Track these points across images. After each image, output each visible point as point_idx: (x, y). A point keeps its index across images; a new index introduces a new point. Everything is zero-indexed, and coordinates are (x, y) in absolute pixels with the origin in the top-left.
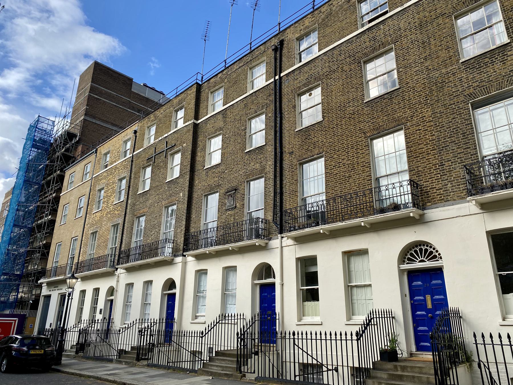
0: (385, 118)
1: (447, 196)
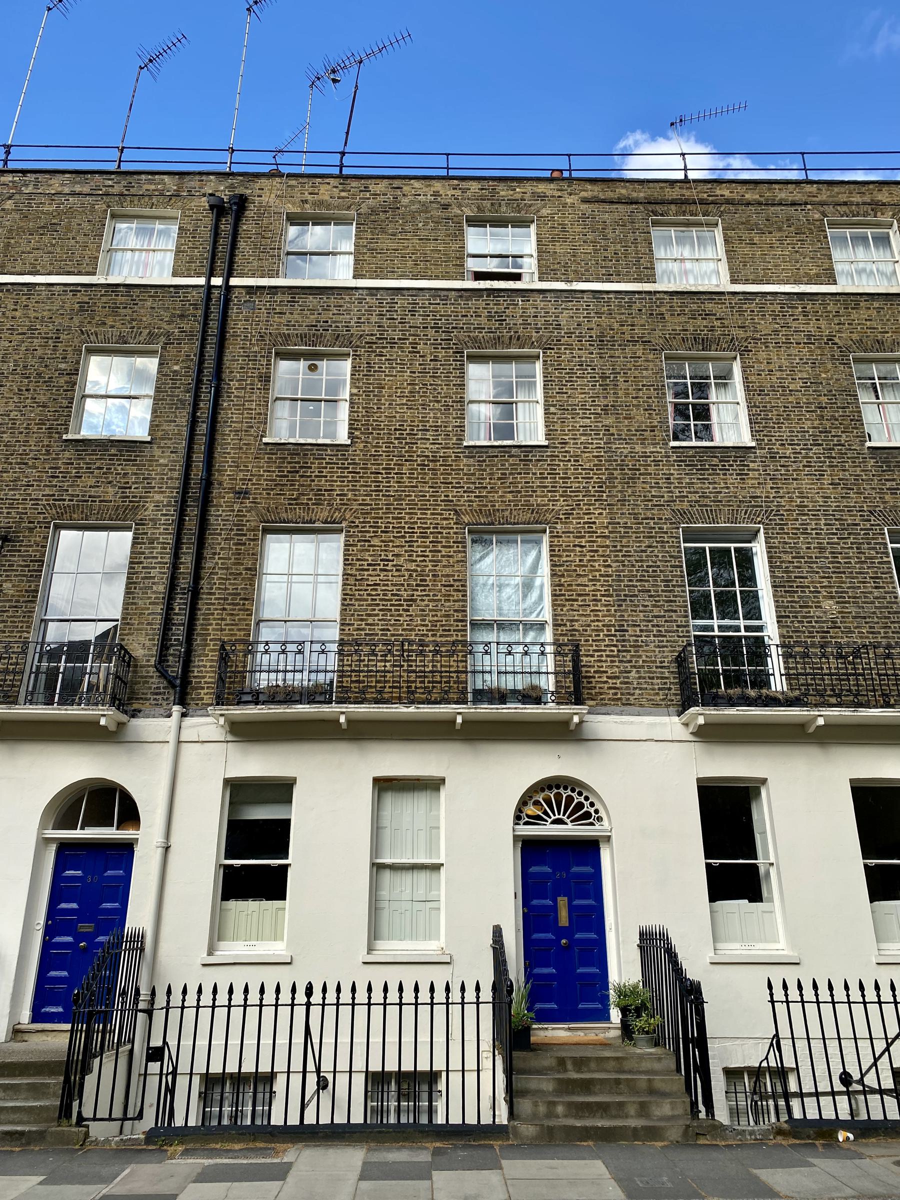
0: (510, 496)
1: (629, 694)
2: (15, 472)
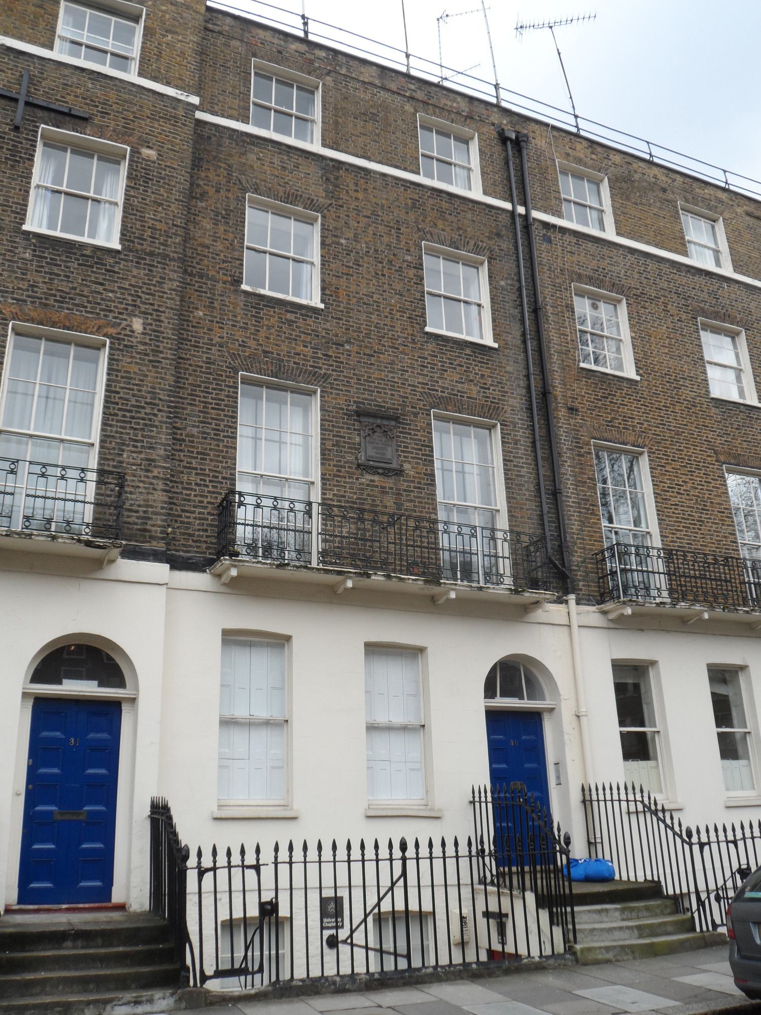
2: (390, 355)
